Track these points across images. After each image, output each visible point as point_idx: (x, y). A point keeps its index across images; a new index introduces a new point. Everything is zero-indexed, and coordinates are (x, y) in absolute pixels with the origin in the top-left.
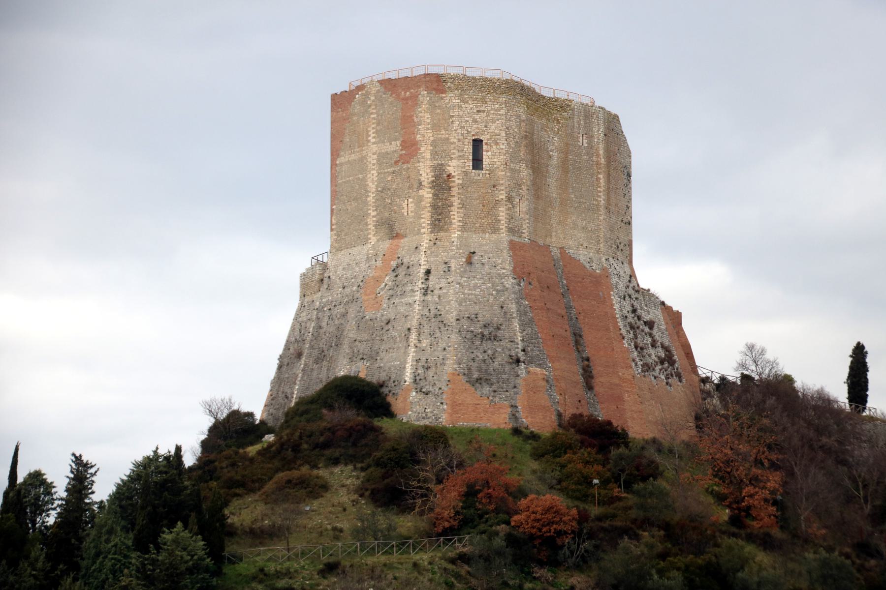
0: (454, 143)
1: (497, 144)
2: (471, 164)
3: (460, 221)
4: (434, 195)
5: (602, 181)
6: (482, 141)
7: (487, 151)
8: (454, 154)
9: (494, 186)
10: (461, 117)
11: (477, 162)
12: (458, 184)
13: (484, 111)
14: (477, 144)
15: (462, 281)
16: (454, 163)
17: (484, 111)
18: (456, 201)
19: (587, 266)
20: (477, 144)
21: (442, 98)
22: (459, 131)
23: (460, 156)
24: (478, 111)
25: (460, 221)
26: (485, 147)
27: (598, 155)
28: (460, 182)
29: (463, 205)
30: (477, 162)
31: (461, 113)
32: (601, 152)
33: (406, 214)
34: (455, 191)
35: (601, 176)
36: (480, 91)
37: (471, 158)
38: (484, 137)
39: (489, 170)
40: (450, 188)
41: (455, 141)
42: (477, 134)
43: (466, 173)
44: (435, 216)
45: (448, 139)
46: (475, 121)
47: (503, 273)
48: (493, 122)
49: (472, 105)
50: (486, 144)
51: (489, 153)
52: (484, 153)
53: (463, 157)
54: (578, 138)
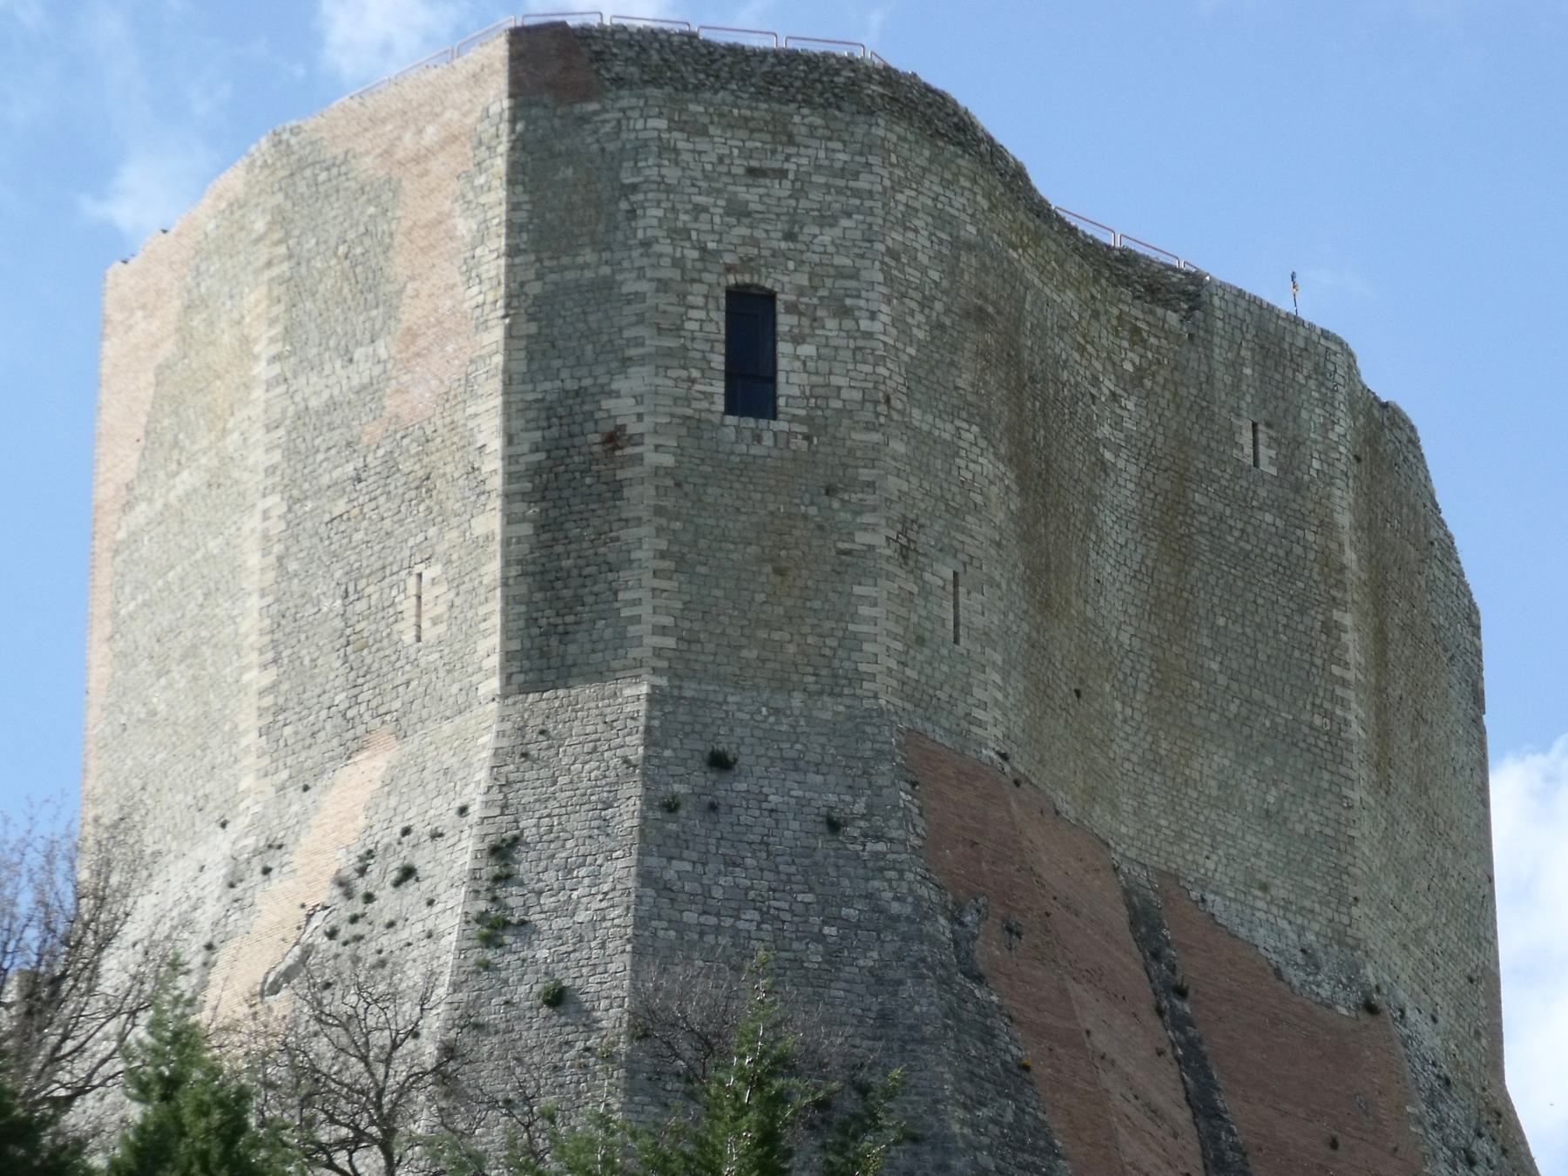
0: (640, 297)
1: (844, 312)
2: (719, 387)
3: (662, 630)
4: (541, 527)
5: (1349, 638)
6: (771, 297)
7: (798, 340)
8: (638, 342)
9: (830, 491)
10: (669, 189)
11: (750, 385)
12: (657, 470)
13: (782, 174)
14: (750, 319)
15: (670, 874)
16: (636, 381)
17: (782, 174)
18: (645, 543)
19: (1295, 976)
20: (750, 319)
21: (584, 119)
22: (664, 247)
23: (669, 353)
24: (751, 172)
25: (662, 630)
26: (785, 322)
27: (1327, 526)
28: (668, 460)
29: (679, 562)
30: (750, 385)
31: (672, 174)
32: (1344, 519)
33: (408, 638)
34: (640, 498)
35: (1348, 620)
36: (762, 93)
37: (718, 361)
38: (784, 283)
39: (808, 420)
40: (617, 488)
41: (643, 286)
42: (746, 263)
43: (695, 426)
44: (547, 617)
45: (608, 285)
46: (738, 211)
47: (876, 855)
48: (826, 219)
49: (719, 145)
50: (792, 308)
51: (807, 350)
52: (783, 347)
53: (680, 356)
54: (1232, 431)
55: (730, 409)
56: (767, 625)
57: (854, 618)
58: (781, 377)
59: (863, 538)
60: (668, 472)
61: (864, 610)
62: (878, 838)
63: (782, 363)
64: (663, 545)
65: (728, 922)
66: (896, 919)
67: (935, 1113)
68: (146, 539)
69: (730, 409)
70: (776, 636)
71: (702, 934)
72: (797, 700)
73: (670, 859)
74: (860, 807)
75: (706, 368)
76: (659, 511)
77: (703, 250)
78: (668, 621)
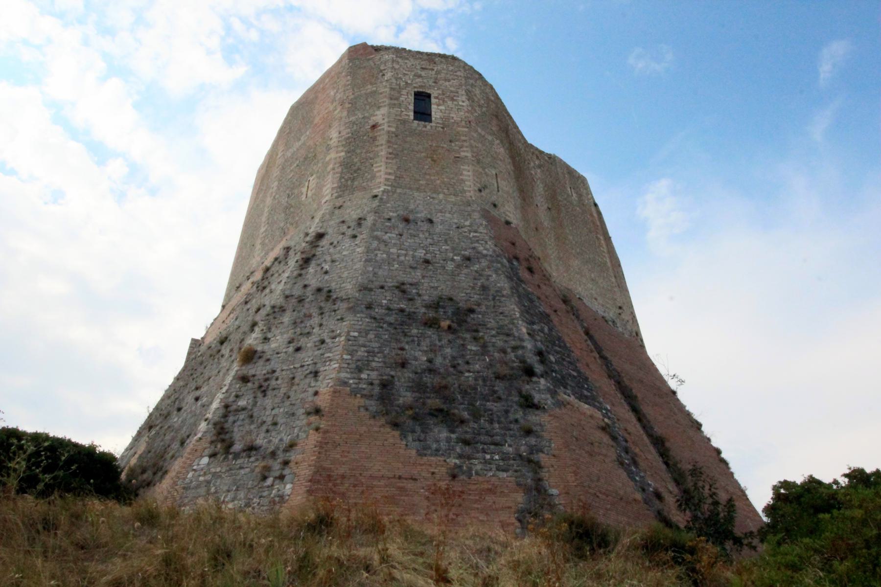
1: (453, 100)
9: (451, 141)
11: (422, 113)
13: (433, 70)
26: (433, 100)
29: (394, 155)
30: (422, 113)
34: (382, 139)
40: (374, 139)
42: (421, 87)
43: (404, 122)
50: (436, 98)
55: (415, 118)
56: (429, 174)
57: (462, 174)
58: (433, 113)
59: (463, 154)
60: (393, 133)
61: (465, 173)
62: (476, 232)
63: (433, 110)
64: (390, 150)
65: (411, 253)
66: (486, 256)
67: (513, 324)
68: (325, 385)
69: (415, 118)
70: (432, 178)
71: (398, 256)
72: (441, 196)
73: (386, 233)
74: (467, 223)
75: (407, 109)
76: (389, 142)
77: (407, 83)
78: (390, 171)
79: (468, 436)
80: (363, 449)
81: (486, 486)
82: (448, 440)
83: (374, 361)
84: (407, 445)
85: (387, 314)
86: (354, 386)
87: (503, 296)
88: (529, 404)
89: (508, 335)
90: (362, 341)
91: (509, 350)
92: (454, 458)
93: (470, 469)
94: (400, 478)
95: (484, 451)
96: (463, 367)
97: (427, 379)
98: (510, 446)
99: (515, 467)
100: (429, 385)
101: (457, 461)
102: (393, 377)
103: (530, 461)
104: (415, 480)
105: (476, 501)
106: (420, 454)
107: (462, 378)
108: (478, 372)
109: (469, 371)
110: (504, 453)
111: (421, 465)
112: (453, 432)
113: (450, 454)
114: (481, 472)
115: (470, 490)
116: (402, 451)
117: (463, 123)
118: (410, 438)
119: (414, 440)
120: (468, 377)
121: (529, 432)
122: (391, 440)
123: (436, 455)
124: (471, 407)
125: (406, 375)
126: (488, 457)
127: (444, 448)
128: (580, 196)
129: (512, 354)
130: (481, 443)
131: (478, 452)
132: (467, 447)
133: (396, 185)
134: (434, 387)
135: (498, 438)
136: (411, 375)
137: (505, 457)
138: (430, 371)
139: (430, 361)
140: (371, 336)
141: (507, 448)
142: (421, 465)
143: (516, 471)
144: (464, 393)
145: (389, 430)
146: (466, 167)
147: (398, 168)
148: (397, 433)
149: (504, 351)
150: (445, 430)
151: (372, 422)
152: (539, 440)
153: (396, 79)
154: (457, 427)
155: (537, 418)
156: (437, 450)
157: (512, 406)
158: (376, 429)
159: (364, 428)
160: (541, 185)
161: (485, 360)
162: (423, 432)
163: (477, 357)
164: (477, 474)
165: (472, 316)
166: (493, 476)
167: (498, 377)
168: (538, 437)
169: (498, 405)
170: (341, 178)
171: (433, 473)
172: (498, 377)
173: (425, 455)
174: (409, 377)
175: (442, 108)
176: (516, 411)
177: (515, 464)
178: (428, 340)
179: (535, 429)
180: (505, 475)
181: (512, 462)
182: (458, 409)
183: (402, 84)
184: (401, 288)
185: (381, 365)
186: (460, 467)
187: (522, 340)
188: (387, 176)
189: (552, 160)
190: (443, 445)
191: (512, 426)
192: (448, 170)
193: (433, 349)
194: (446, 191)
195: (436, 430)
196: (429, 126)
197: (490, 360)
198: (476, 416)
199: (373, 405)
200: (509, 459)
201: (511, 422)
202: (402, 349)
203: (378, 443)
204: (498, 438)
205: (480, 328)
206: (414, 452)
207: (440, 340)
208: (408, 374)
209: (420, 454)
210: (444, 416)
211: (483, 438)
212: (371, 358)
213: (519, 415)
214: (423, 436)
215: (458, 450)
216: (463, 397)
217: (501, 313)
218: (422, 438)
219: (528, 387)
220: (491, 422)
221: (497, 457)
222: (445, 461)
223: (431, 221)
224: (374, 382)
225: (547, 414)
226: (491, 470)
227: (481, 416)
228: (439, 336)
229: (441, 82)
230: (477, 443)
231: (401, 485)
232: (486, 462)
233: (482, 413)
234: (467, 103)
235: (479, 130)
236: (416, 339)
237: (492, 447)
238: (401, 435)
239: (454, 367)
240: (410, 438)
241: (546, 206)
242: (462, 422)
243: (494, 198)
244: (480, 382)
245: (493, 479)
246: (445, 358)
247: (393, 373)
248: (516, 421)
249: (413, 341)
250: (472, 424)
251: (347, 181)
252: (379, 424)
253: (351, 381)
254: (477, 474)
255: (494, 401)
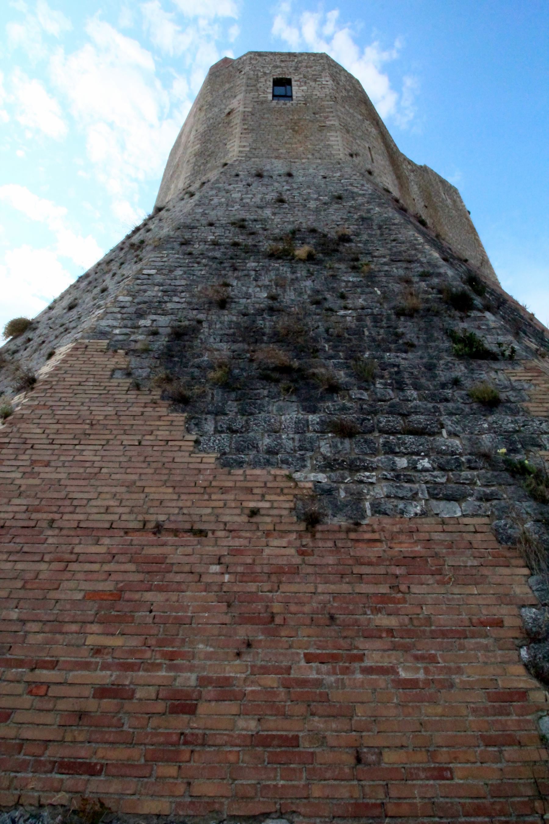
1: (315, 81)
29: (247, 131)
56: (291, 144)
70: (294, 146)
79: (349, 418)
80: (88, 455)
81: (405, 547)
82: (301, 428)
83: (171, 301)
84: (197, 442)
85: (214, 250)
86: (120, 338)
87: (394, 224)
88: (473, 351)
89: (410, 262)
90: (159, 279)
91: (416, 279)
92: (314, 469)
93: (359, 498)
94: (158, 529)
95: (390, 450)
96: (332, 301)
97: (266, 323)
98: (453, 434)
99: (479, 488)
100: (267, 331)
101: (322, 477)
102: (200, 322)
103: (519, 471)
104: (202, 533)
105: (380, 603)
106: (226, 463)
107: (333, 318)
108: (363, 308)
109: (346, 308)
110: (440, 452)
111: (224, 490)
112: (314, 411)
113: (303, 459)
114: (388, 506)
115: (359, 561)
116: (182, 457)
117: (328, 98)
118: (209, 427)
119: (217, 431)
120: (344, 316)
121: (490, 403)
122: (163, 434)
123: (268, 463)
124: (352, 362)
125: (226, 318)
126: (402, 462)
127: (289, 445)
128: (454, 202)
129: (423, 284)
130: (381, 431)
131: (375, 452)
132: (347, 441)
133: (251, 155)
134: (276, 334)
135: (421, 418)
136: (234, 319)
137: (447, 463)
138: (271, 310)
139: (273, 298)
140: (179, 272)
141: (444, 441)
142: (224, 490)
143: (487, 498)
144: (337, 339)
145: (163, 411)
146: (332, 134)
147: (255, 141)
148: (180, 418)
149: (408, 281)
150: (294, 406)
151: (132, 396)
152: (520, 418)
153: (254, 71)
154: (322, 399)
155: (501, 376)
156: (271, 451)
157: (439, 358)
158: (136, 410)
159: (110, 410)
160: (415, 186)
161: (375, 292)
162: (243, 412)
163: (359, 290)
164: (377, 509)
165: (347, 245)
166: (424, 514)
167: (400, 313)
168: (514, 412)
169: (410, 355)
170: (195, 165)
171: (254, 513)
172: (400, 313)
173: (240, 464)
174: (231, 321)
175: (305, 88)
176: (448, 367)
177: (478, 478)
178: (272, 274)
179: (503, 396)
180: (456, 510)
181: (466, 474)
182: (324, 366)
183: (260, 74)
184: (241, 225)
185: (184, 306)
186: (329, 492)
187: (436, 266)
188: (241, 149)
189: (424, 170)
190: (289, 440)
191: (448, 392)
192: (312, 138)
193: (280, 283)
194: (310, 156)
195: (273, 408)
196: (289, 104)
197: (383, 293)
198: (365, 378)
199: (143, 368)
200: (459, 465)
201: (443, 386)
202: (226, 285)
203: (127, 440)
204: (419, 420)
205: (360, 256)
206: (211, 458)
207: (293, 273)
208: (229, 317)
209: (226, 463)
210: (297, 382)
211: (383, 420)
212: (166, 298)
213: (460, 370)
214: (241, 421)
215: (325, 448)
216: (334, 347)
217: (394, 240)
218: (236, 426)
219: (465, 325)
220: (400, 386)
221: (425, 463)
222: (289, 478)
223: (290, 175)
224: (161, 330)
225: (519, 369)
226: (414, 497)
227: (374, 377)
228: (292, 268)
229: (302, 69)
230: (371, 432)
231: (155, 551)
232: (398, 477)
233: (377, 371)
234: (330, 82)
235: (347, 107)
236: (253, 273)
237: (410, 439)
238: (188, 420)
239: (317, 303)
240: (209, 427)
241: (423, 204)
242: (334, 389)
243: (369, 167)
244: (368, 321)
245: (427, 523)
246: (300, 294)
247: (201, 316)
248: (456, 382)
249: (248, 275)
250: (355, 393)
251: (200, 166)
252: (144, 399)
253: (117, 331)
254: (377, 509)
255: (399, 350)
